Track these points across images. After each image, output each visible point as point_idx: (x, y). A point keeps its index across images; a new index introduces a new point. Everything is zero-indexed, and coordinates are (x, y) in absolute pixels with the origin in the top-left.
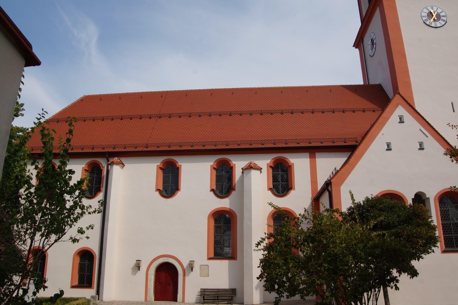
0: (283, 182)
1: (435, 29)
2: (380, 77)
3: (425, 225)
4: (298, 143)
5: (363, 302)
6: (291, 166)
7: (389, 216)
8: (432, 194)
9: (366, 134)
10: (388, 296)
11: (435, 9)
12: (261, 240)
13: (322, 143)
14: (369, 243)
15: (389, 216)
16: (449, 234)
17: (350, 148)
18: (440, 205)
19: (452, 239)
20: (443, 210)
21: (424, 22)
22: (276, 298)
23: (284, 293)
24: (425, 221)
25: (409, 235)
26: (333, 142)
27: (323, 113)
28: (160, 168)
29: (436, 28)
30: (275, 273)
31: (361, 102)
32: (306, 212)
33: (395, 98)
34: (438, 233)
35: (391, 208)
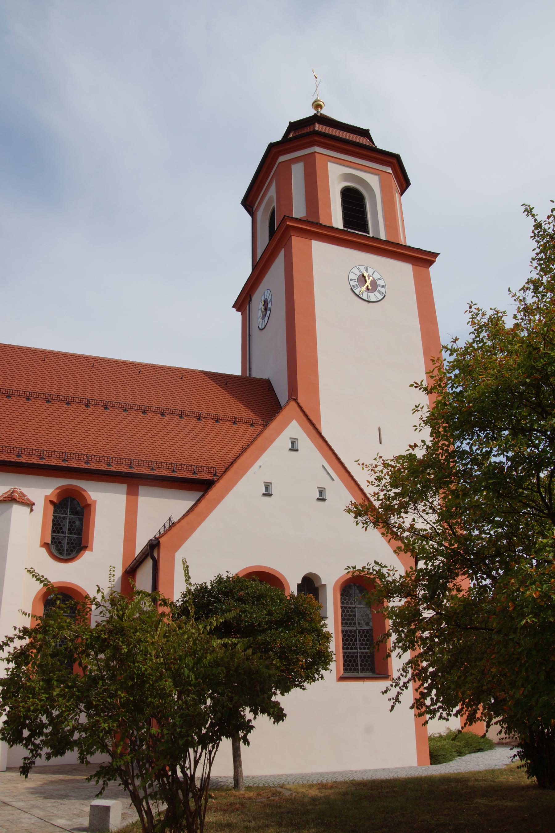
0: (71, 533)
1: (366, 303)
2: (271, 368)
3: (313, 632)
4: (109, 465)
5: (187, 765)
6: (90, 505)
7: (254, 612)
8: (331, 577)
9: (232, 464)
10: (239, 756)
11: (371, 271)
12: (5, 640)
13: (152, 469)
14: (206, 658)
15: (254, 612)
16: (351, 648)
17: (201, 485)
18: (341, 599)
19: (357, 657)
20: (345, 608)
21: (352, 289)
22: (25, 759)
23: (41, 749)
24: (313, 625)
25: (284, 647)
26: (173, 471)
27: (163, 415)
28: (52, 502)
29: (369, 302)
30: (23, 707)
31: (236, 408)
32: (100, 594)
33: (288, 408)
34: (334, 646)
35: (259, 598)
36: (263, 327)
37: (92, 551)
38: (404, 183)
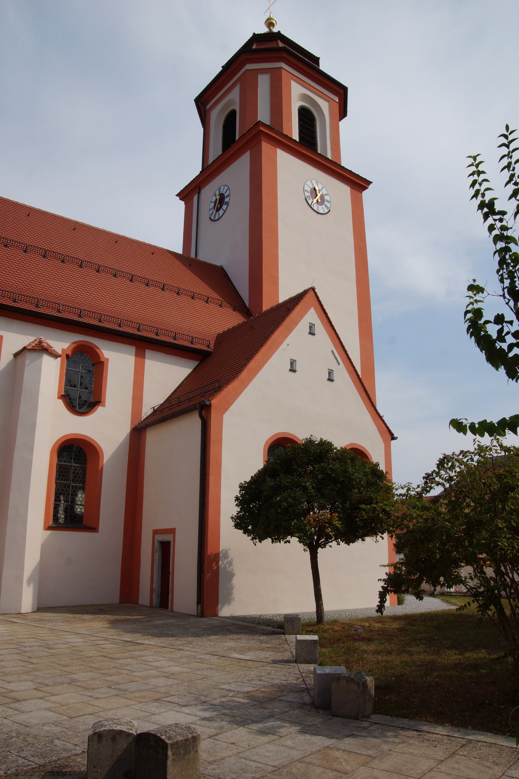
1: (316, 213)
4: (15, 301)
29: (318, 213)
36: (217, 218)
37: (104, 406)
38: (343, 113)
